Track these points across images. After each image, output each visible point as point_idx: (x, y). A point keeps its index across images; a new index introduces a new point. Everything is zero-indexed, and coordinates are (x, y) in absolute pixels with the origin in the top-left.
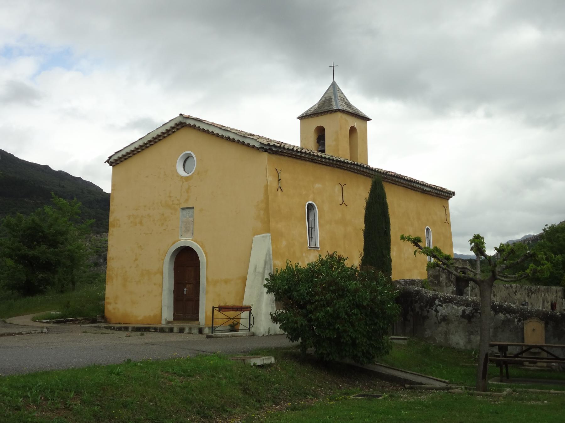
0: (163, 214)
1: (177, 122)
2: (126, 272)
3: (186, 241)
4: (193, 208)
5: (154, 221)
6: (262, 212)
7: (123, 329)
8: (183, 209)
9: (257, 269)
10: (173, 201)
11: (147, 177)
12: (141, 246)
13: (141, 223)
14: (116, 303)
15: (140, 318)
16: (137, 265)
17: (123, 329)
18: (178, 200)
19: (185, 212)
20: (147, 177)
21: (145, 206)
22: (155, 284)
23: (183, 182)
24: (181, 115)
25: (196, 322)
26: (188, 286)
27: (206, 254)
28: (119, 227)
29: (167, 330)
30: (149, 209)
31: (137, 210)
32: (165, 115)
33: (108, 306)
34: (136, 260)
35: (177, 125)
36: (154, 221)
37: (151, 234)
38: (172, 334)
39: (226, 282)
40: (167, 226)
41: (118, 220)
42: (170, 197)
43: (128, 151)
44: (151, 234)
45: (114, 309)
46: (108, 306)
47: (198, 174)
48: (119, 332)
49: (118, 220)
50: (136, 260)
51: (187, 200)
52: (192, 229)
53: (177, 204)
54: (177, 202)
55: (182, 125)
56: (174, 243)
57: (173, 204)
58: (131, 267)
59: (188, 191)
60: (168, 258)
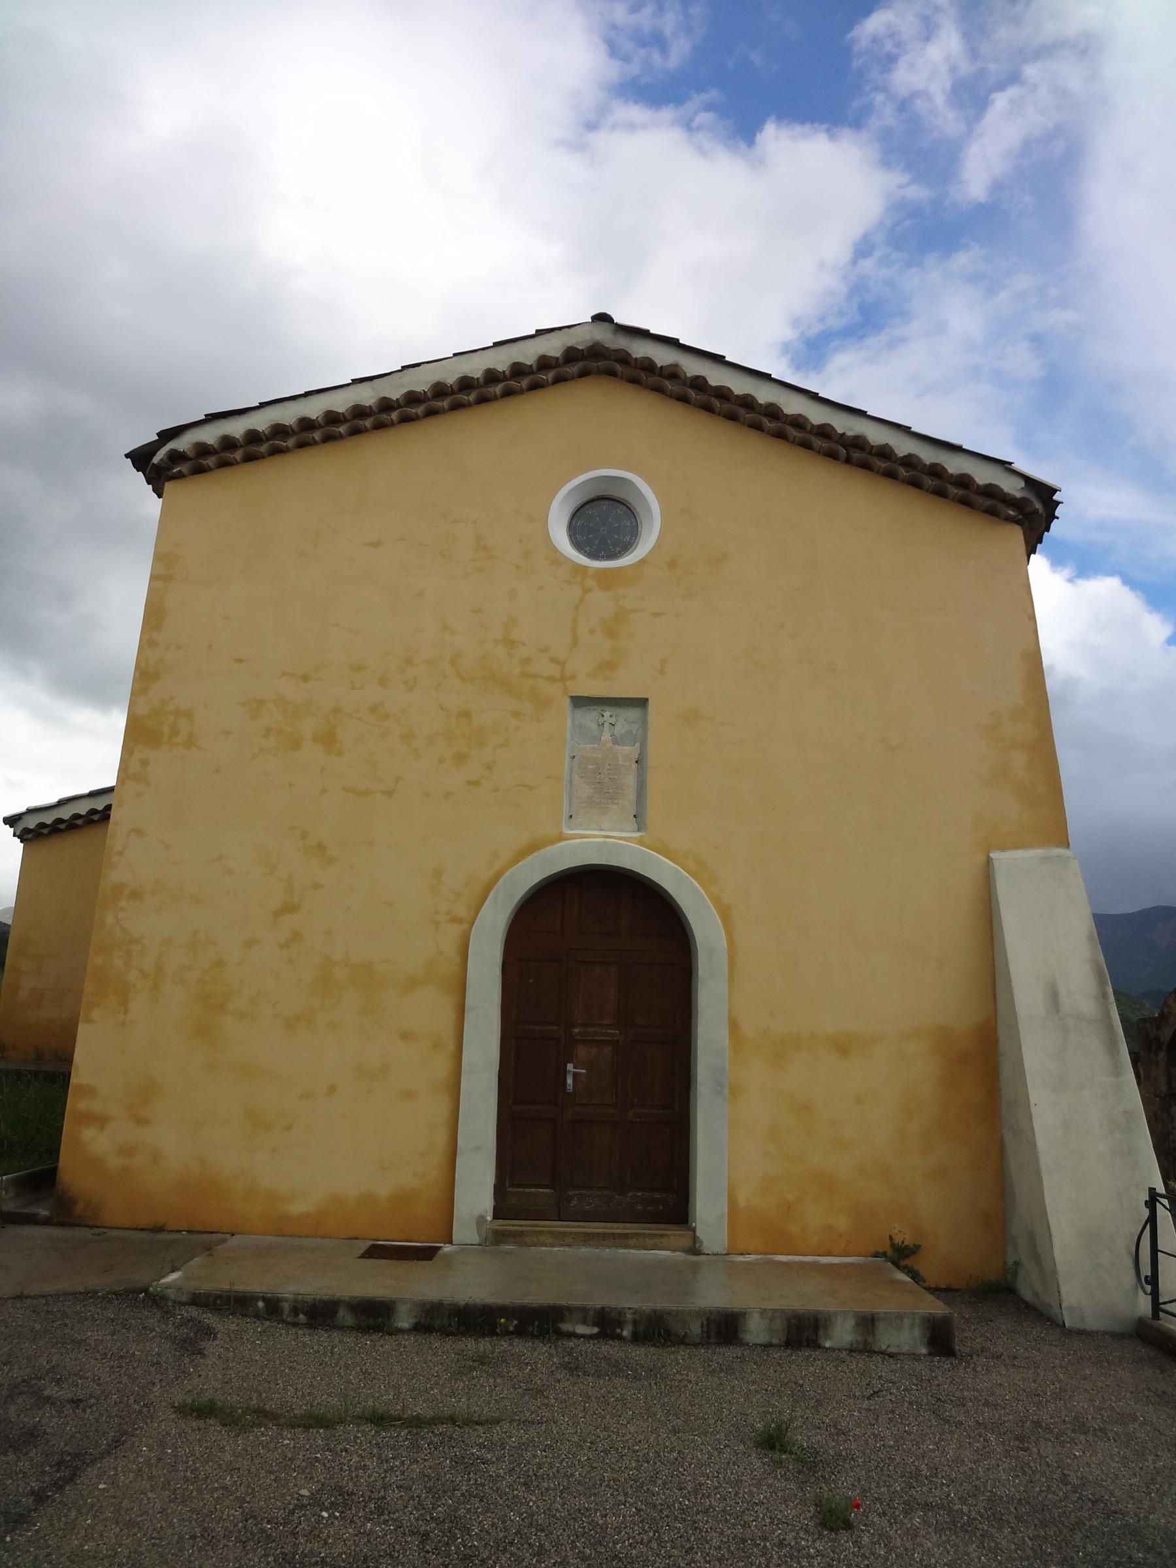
0: (466, 715)
1: (581, 340)
2: (220, 964)
3: (600, 840)
4: (642, 703)
5: (408, 736)
6: (1019, 759)
7: (345, 1317)
8: (579, 702)
9: (1066, 1002)
10: (526, 661)
11: (376, 545)
12: (321, 848)
13: (328, 739)
14: (142, 1121)
15: (297, 1208)
16: (297, 936)
17: (345, 1317)
18: (554, 660)
19: (589, 718)
20: (376, 545)
21: (358, 668)
22: (405, 1036)
23: (587, 591)
24: (602, 318)
25: (676, 1235)
26: (582, 1052)
27: (725, 912)
28: (189, 744)
29: (695, 1329)
30: (383, 682)
31: (306, 678)
32: (546, 301)
33: (88, 1134)
34: (289, 908)
35: (571, 355)
36: (408, 736)
37: (390, 794)
38: (730, 1352)
39: (843, 1046)
40: (489, 767)
41: (189, 715)
42: (510, 643)
43: (341, 409)
44: (390, 794)
45: (127, 1151)
46: (88, 1134)
47: (672, 565)
48: (322, 1338)
49: (189, 715)
50: (289, 908)
51: (607, 667)
52: (631, 794)
53: (551, 679)
54: (555, 670)
55: (606, 360)
56: (532, 848)
57: (525, 675)
58: (250, 943)
59: (613, 627)
60: (495, 920)
